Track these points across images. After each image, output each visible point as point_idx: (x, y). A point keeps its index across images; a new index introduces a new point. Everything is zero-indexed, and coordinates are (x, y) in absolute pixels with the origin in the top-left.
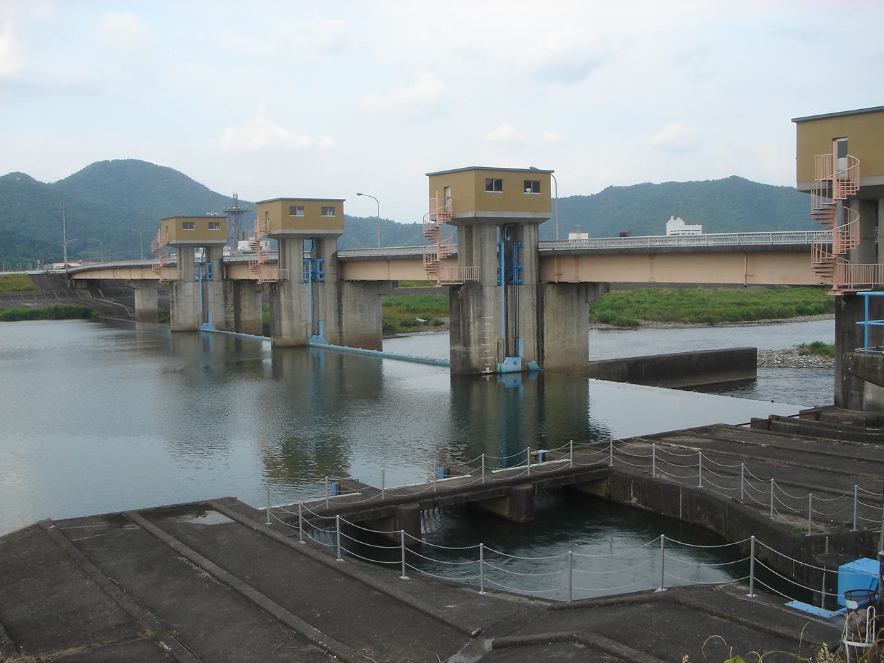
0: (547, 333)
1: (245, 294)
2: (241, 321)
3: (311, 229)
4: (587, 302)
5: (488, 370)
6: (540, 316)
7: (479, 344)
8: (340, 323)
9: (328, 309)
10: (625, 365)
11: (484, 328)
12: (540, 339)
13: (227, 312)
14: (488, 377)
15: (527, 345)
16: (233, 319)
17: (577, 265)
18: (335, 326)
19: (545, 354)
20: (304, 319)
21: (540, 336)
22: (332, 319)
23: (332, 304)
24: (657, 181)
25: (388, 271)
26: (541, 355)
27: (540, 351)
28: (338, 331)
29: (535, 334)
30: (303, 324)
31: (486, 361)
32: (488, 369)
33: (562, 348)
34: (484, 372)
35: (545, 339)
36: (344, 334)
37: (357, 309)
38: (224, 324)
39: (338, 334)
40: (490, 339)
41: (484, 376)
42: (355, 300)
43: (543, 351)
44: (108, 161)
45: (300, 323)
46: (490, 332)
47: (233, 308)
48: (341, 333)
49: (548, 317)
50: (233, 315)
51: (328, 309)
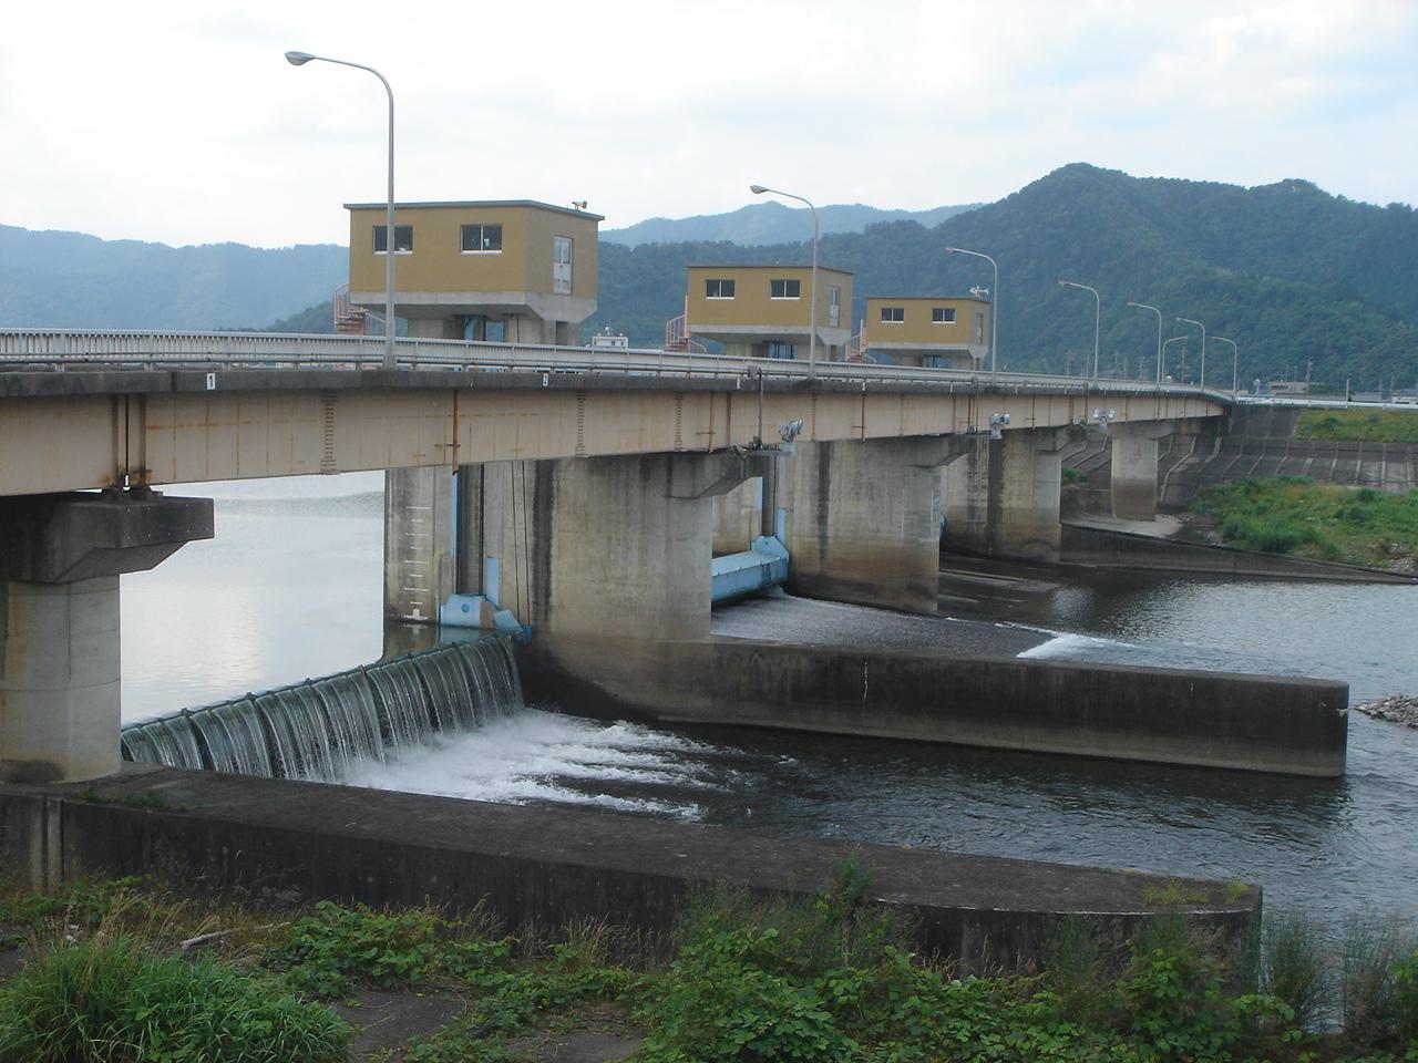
0: (560, 557)
1: (1013, 455)
2: (1001, 509)
3: (892, 341)
4: (669, 496)
5: (416, 615)
6: (541, 515)
7: (400, 560)
8: (822, 519)
9: (798, 487)
10: (804, 661)
11: (410, 528)
12: (542, 567)
13: (973, 488)
14: (416, 629)
15: (505, 576)
16: (985, 505)
17: (329, 415)
18: (813, 522)
19: (554, 600)
20: (748, 503)
21: (541, 558)
22: (805, 507)
23: (807, 478)
24: (1320, 187)
25: (581, 417)
26: (542, 600)
27: (542, 592)
28: (817, 533)
29: (530, 554)
30: (744, 511)
31: (413, 596)
32: (416, 611)
33: (598, 592)
34: (409, 617)
35: (553, 568)
36: (831, 541)
37: (863, 491)
38: (965, 511)
39: (816, 539)
40: (423, 551)
41: (409, 626)
42: (859, 474)
43: (548, 594)
44: (783, 245)
45: (739, 510)
46: (423, 539)
47: (986, 482)
48: (823, 537)
49: (561, 520)
50: (985, 495)
51: (798, 487)
